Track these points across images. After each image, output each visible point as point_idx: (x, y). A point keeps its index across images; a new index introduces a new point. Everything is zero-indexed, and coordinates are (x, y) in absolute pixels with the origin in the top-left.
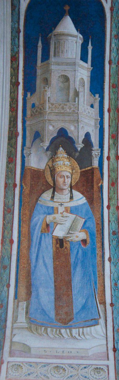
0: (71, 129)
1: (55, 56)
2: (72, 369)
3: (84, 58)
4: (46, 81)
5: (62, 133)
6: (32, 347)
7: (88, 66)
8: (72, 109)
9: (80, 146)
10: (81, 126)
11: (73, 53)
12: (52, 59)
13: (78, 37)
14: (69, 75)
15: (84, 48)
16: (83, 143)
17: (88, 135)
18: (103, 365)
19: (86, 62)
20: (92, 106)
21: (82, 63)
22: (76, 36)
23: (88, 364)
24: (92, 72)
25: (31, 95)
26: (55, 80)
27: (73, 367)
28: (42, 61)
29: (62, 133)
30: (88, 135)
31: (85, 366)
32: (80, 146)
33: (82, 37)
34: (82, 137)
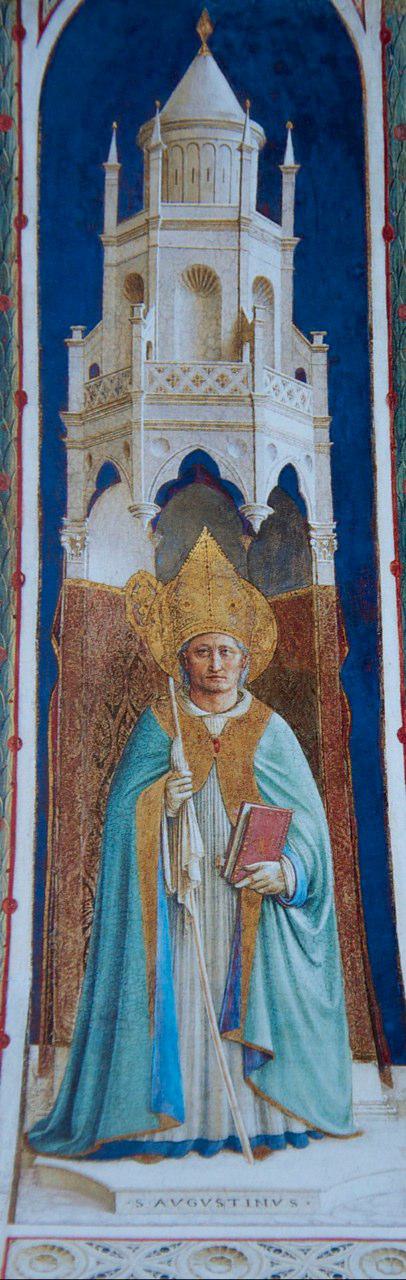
0: (228, 461)
1: (166, 197)
2: (277, 1256)
3: (269, 204)
4: (136, 287)
5: (198, 468)
6: (125, 1190)
7: (284, 231)
8: (232, 386)
9: (260, 512)
10: (263, 441)
11: (367, 1120)
12: (158, 206)
13: (248, 129)
14: (220, 266)
15: (270, 157)
16: (270, 503)
17: (289, 475)
18: (291, 1240)
19: (276, 217)
20: (301, 375)
21: (263, 222)
22: (242, 129)
23: (176, 1236)
24: (299, 255)
25: (85, 334)
26: (166, 277)
27: (280, 1251)
28: (121, 219)
29: (198, 468)
30: (289, 475)
31: (335, 1244)
32: (260, 512)
33: (260, 129)
34: (269, 480)
